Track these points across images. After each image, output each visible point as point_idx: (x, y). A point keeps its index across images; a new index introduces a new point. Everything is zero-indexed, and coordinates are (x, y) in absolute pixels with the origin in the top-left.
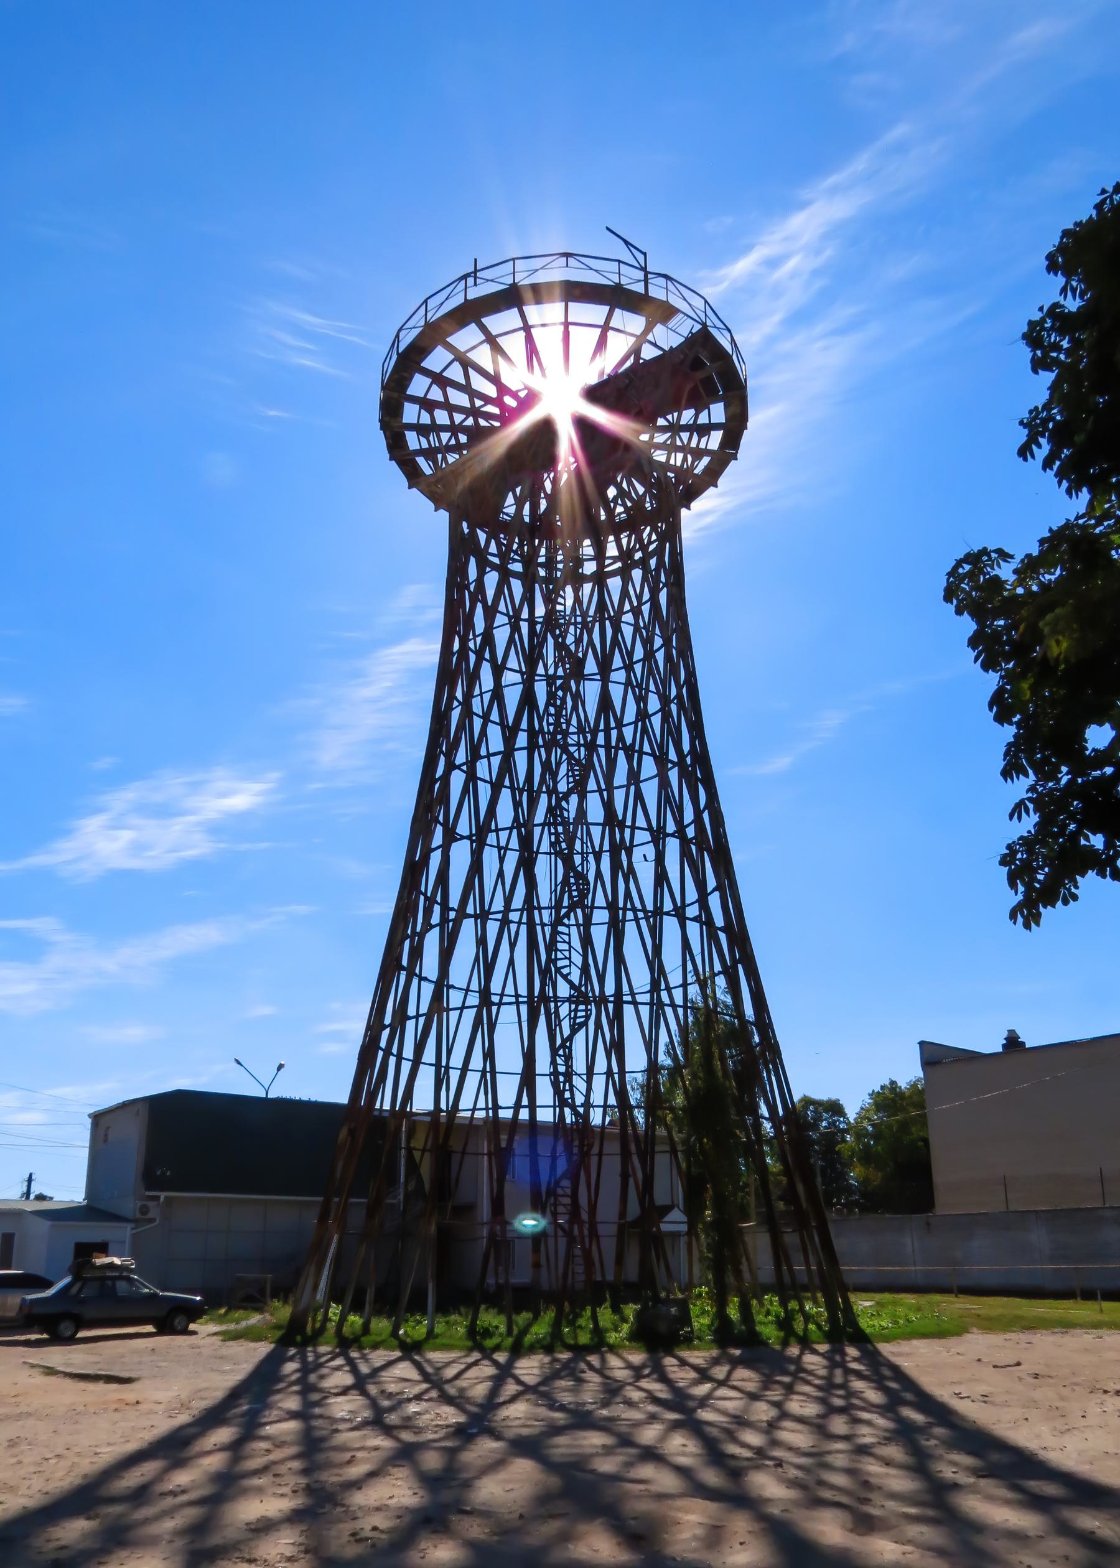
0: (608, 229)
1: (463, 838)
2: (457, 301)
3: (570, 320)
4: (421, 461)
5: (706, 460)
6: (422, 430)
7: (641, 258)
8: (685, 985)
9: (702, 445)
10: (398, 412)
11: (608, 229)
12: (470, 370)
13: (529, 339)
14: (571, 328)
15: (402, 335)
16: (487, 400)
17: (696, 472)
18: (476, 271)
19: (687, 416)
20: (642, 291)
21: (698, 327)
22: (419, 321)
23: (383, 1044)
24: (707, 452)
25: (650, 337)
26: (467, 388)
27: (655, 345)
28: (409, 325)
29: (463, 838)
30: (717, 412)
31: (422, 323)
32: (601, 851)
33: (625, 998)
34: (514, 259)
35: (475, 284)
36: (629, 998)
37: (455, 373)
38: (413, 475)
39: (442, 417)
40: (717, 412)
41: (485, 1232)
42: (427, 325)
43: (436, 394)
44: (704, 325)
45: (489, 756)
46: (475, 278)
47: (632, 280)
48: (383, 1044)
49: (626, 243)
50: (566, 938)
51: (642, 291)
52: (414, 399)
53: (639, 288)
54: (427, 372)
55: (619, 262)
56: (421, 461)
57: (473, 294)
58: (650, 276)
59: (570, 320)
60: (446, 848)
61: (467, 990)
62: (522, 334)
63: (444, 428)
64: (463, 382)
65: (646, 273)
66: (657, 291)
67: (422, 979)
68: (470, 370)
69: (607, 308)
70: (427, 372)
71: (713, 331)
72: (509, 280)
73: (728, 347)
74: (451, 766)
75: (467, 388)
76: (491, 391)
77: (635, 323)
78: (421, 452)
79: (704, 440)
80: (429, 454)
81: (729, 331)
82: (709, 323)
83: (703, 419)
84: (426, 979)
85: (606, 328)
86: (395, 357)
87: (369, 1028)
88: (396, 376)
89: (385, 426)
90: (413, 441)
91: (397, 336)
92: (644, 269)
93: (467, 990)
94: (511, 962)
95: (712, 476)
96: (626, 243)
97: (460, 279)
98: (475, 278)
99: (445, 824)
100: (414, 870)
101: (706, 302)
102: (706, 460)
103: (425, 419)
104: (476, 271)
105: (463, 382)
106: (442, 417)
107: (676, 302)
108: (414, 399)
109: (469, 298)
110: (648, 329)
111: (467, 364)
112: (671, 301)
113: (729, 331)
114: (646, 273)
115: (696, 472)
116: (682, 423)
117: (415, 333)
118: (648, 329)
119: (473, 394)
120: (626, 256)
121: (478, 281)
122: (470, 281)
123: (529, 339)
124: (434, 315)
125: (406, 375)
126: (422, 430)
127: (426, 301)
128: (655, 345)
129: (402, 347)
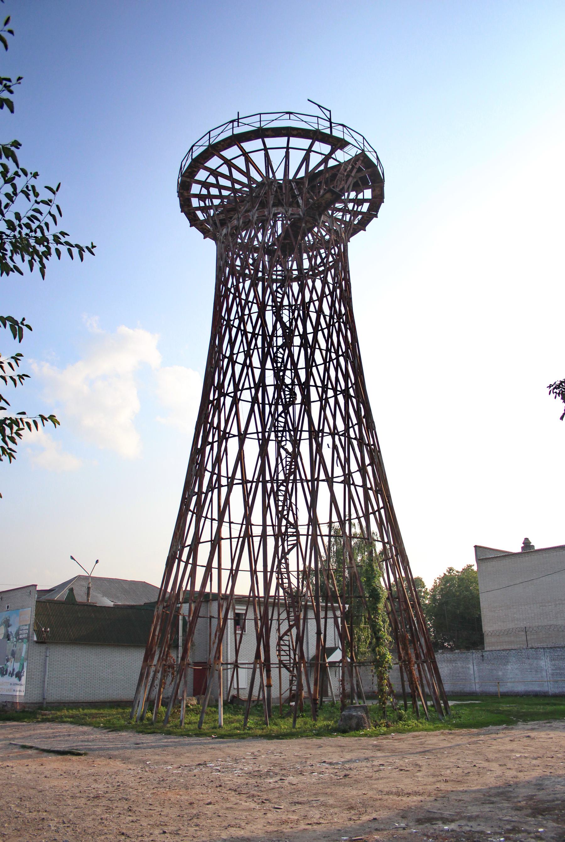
0: (309, 100)
1: (234, 436)
2: (228, 134)
3: (290, 146)
4: (199, 213)
6: (200, 197)
7: (327, 113)
10: (189, 188)
11: (309, 100)
12: (232, 169)
14: (290, 150)
15: (194, 148)
18: (238, 119)
19: (353, 195)
20: (329, 133)
21: (360, 152)
22: (205, 142)
24: (361, 213)
25: (333, 156)
26: (230, 178)
27: (336, 160)
28: (200, 143)
29: (234, 436)
30: (368, 194)
31: (207, 144)
34: (260, 114)
35: (238, 126)
38: (194, 221)
39: (214, 191)
40: (368, 194)
41: (354, 714)
42: (210, 146)
44: (363, 150)
45: (250, 388)
46: (238, 122)
47: (324, 127)
49: (319, 106)
51: (329, 133)
52: (198, 182)
53: (328, 131)
54: (207, 169)
55: (318, 117)
56: (199, 213)
57: (237, 131)
58: (333, 125)
59: (290, 146)
62: (263, 152)
63: (216, 197)
64: (228, 174)
65: (331, 123)
66: (337, 133)
68: (232, 169)
71: (368, 154)
72: (258, 125)
73: (375, 161)
75: (230, 178)
76: (245, 180)
78: (199, 208)
79: (360, 207)
80: (204, 210)
81: (376, 152)
82: (365, 150)
83: (360, 196)
85: (309, 151)
86: (190, 160)
88: (190, 170)
89: (180, 195)
90: (195, 202)
91: (192, 148)
92: (330, 120)
94: (211, 500)
95: (362, 226)
96: (319, 106)
97: (287, 113)
98: (238, 122)
100: (197, 454)
101: (364, 138)
103: (204, 192)
104: (238, 119)
105: (228, 174)
106: (214, 191)
107: (348, 138)
109: (235, 133)
110: (333, 151)
112: (346, 139)
113: (376, 152)
114: (331, 123)
116: (350, 198)
117: (202, 149)
119: (234, 181)
120: (319, 113)
121: (240, 124)
122: (236, 124)
124: (214, 141)
125: (196, 170)
126: (200, 197)
127: (209, 132)
128: (336, 160)
129: (195, 155)
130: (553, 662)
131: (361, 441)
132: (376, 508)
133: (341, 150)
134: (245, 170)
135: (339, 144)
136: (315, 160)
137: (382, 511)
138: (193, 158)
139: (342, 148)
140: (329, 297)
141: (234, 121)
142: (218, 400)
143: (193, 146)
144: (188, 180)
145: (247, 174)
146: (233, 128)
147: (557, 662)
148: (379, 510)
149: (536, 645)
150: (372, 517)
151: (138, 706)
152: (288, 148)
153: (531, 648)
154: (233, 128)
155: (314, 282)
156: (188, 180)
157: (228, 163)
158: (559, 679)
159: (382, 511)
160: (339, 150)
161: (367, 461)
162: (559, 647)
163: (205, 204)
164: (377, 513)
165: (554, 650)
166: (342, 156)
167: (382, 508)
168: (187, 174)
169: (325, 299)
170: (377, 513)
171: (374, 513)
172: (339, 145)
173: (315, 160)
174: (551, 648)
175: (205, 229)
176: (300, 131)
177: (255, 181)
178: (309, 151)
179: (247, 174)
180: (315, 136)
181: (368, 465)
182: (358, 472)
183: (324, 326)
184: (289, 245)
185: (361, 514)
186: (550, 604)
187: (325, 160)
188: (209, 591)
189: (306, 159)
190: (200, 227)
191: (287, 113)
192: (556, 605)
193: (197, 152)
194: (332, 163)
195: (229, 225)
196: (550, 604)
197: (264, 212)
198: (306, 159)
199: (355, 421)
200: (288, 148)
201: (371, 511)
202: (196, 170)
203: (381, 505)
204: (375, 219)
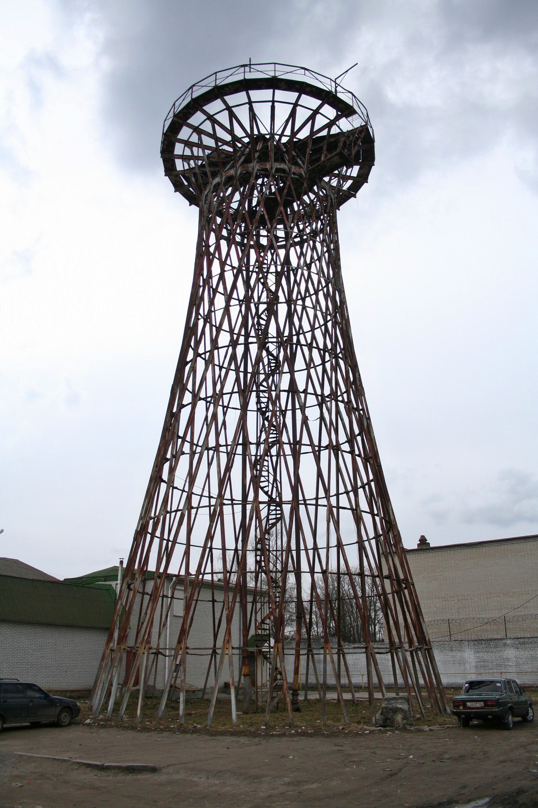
2: (240, 77)
3: (275, 100)
5: (350, 182)
8: (338, 495)
9: (348, 174)
13: (251, 110)
14: (276, 104)
16: (225, 143)
17: (344, 188)
21: (364, 124)
22: (210, 84)
23: (150, 530)
24: (350, 178)
25: (337, 123)
26: (213, 136)
27: (339, 127)
30: (355, 171)
32: (286, 409)
33: (300, 502)
36: (303, 502)
37: (207, 127)
38: (170, 170)
40: (355, 171)
43: (195, 138)
44: (366, 123)
48: (150, 530)
50: (267, 468)
52: (181, 141)
54: (190, 126)
57: (249, 76)
59: (275, 100)
60: (194, 404)
61: (201, 496)
67: (174, 488)
68: (216, 125)
69: (272, 90)
70: (190, 126)
74: (181, 406)
75: (213, 136)
76: (228, 138)
77: (330, 112)
79: (350, 170)
84: (176, 488)
85: (316, 112)
86: (188, 100)
87: (141, 518)
88: (185, 111)
91: (191, 87)
93: (201, 496)
99: (193, 393)
100: (172, 417)
102: (350, 182)
103: (188, 152)
107: (356, 108)
108: (181, 141)
110: (338, 118)
111: (232, 116)
115: (344, 188)
118: (338, 118)
121: (252, 70)
122: (247, 69)
123: (251, 110)
124: (220, 82)
125: (191, 111)
126: (184, 158)
127: (216, 73)
128: (339, 127)
129: (195, 95)
130: (477, 655)
131: (350, 410)
132: (365, 481)
133: (346, 118)
134: (229, 128)
135: (345, 110)
136: (320, 121)
137: (373, 484)
138: (193, 97)
139: (347, 116)
140: (317, 262)
141: (246, 65)
142: (211, 352)
143: (194, 85)
144: (181, 122)
145: (231, 132)
146: (244, 72)
147: (481, 654)
148: (369, 484)
149: (459, 638)
150: (361, 491)
151: (354, 648)
152: (296, 105)
153: (455, 641)
154: (244, 72)
155: (302, 248)
156: (181, 122)
157: (211, 118)
158: (483, 671)
159: (373, 484)
160: (344, 118)
161: (357, 431)
162: (483, 640)
163: (192, 152)
164: (367, 487)
165: (478, 643)
166: (345, 125)
167: (372, 481)
168: (181, 115)
169: (313, 265)
170: (367, 487)
171: (363, 487)
172: (346, 113)
173: (320, 121)
174: (476, 640)
175: (179, 182)
176: (314, 89)
177: (239, 140)
178: (316, 112)
179: (231, 132)
180: (328, 97)
181: (358, 435)
182: (347, 444)
183: (312, 292)
184: (273, 210)
185: (349, 488)
186: (453, 599)
187: (329, 126)
188: (154, 570)
189: (312, 118)
190: (174, 179)
191: (302, 68)
192: (458, 600)
193: (198, 92)
194: (334, 130)
195: (224, 174)
196: (453, 599)
197: (266, 166)
198: (312, 118)
199: (344, 389)
200: (296, 105)
201: (359, 484)
202: (191, 111)
203: (371, 477)
204: (353, 198)
